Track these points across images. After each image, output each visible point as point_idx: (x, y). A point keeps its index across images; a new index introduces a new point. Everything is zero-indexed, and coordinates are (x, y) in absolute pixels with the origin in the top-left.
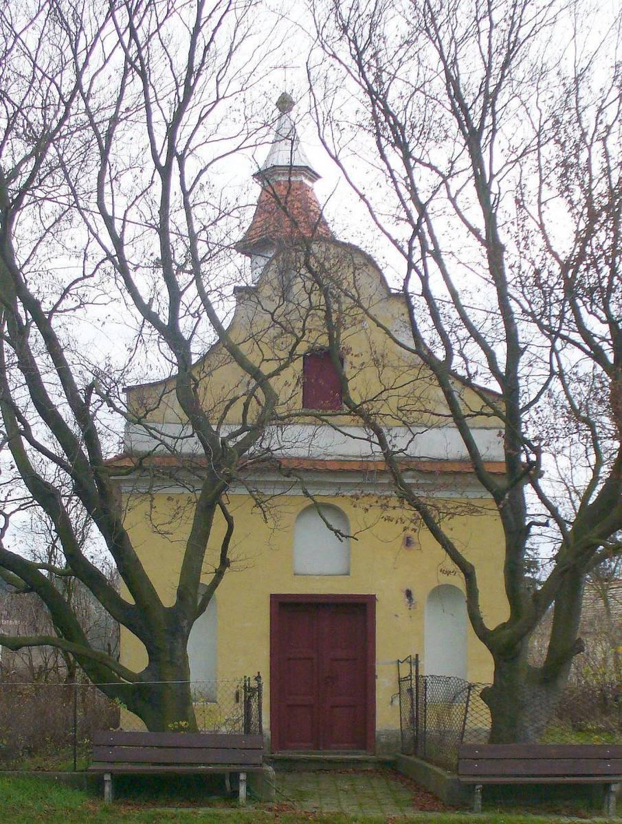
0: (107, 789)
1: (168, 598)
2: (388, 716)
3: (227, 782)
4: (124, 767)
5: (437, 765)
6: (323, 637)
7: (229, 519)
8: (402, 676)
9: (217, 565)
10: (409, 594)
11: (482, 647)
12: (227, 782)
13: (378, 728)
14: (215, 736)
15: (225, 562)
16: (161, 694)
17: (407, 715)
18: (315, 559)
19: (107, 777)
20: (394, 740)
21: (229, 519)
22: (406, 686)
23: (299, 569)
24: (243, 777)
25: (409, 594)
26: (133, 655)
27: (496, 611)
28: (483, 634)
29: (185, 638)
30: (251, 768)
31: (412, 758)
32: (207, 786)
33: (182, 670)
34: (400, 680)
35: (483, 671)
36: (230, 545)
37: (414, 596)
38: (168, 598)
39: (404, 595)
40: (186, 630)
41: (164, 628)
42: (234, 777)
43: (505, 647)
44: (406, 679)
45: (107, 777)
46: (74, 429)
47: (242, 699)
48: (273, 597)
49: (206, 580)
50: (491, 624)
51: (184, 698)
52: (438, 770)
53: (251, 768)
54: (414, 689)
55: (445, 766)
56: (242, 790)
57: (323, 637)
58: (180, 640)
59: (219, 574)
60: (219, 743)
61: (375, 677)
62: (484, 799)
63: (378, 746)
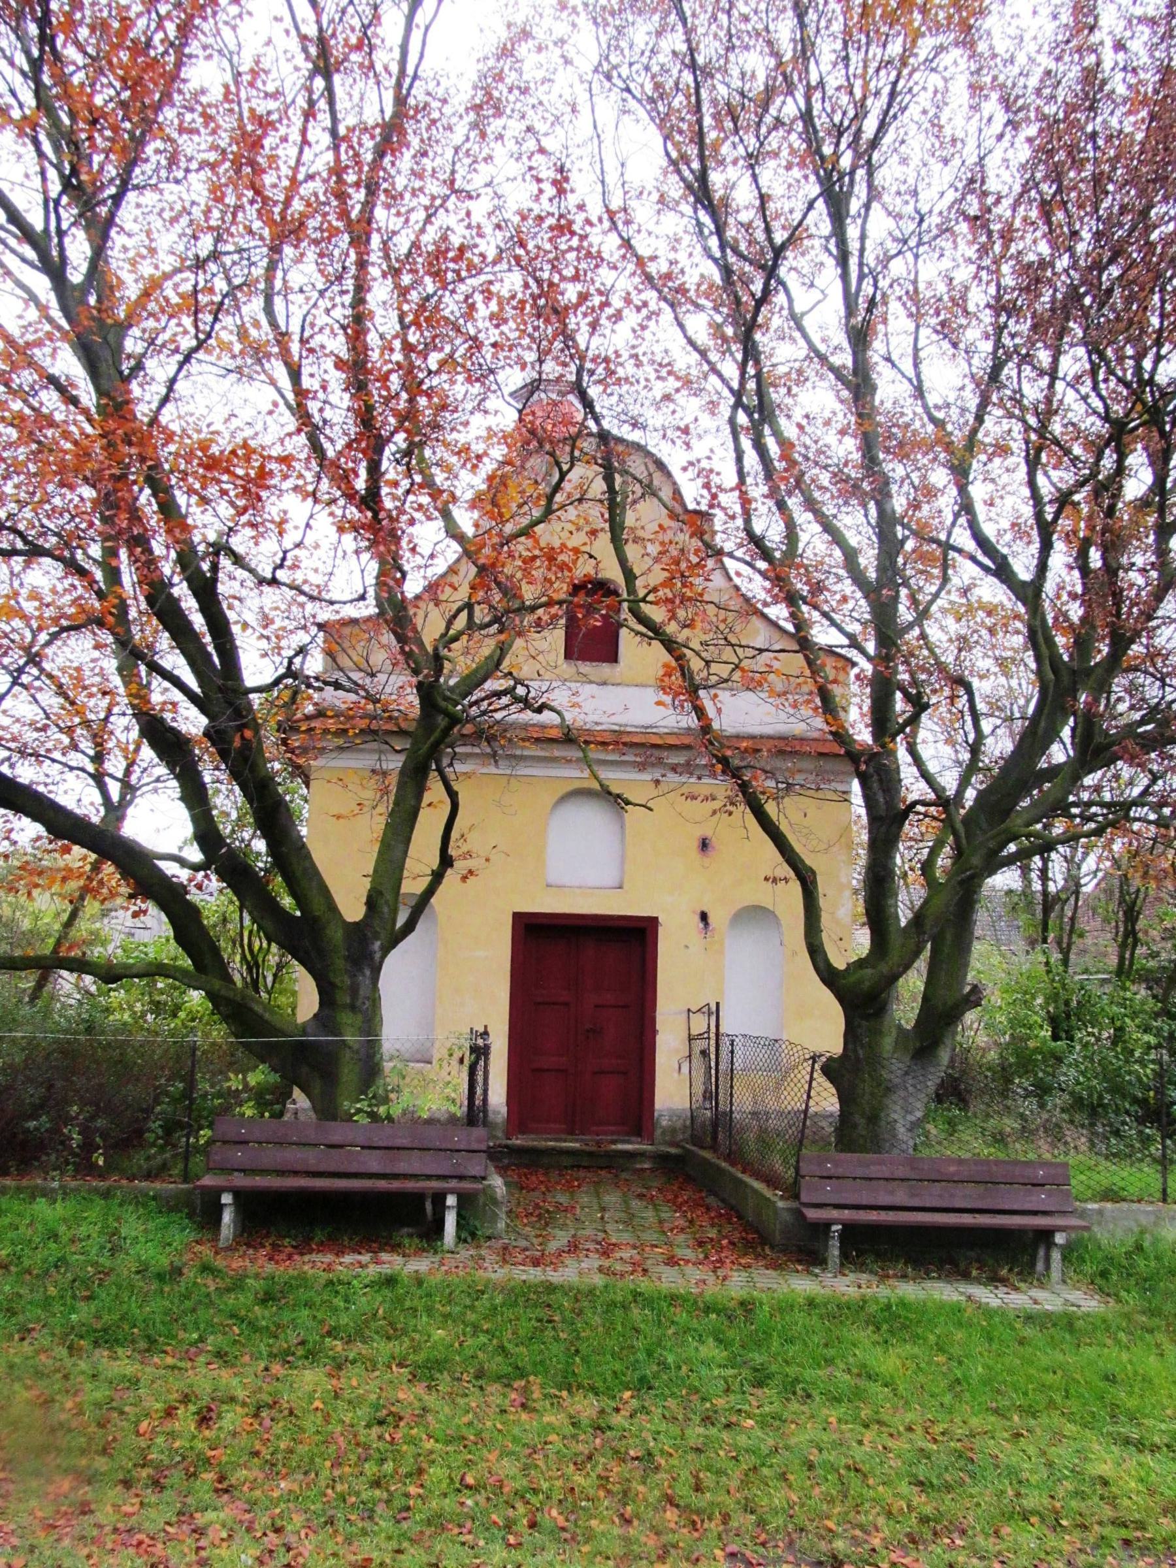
0: (227, 1217)
1: (352, 909)
2: (673, 1091)
3: (429, 1207)
4: (259, 1181)
5: (758, 1176)
6: (584, 972)
7: (453, 795)
8: (694, 1032)
9: (435, 863)
10: (704, 917)
11: (827, 997)
12: (429, 1207)
13: (658, 1105)
14: (414, 1121)
15: (446, 861)
16: (328, 1062)
17: (699, 1089)
18: (581, 864)
19: (226, 1199)
20: (679, 1124)
21: (453, 795)
22: (699, 1045)
23: (553, 878)
24: (451, 1200)
25: (704, 917)
26: (302, 997)
27: (850, 942)
28: (829, 976)
29: (377, 970)
30: (466, 1185)
31: (707, 1154)
32: (388, 1215)
33: (371, 1022)
34: (691, 1039)
35: (824, 1028)
36: (454, 835)
37: (711, 920)
38: (352, 909)
39: (697, 918)
40: (377, 956)
41: (347, 955)
42: (439, 1199)
43: (861, 996)
44: (700, 1036)
45: (226, 1199)
46: (198, 621)
47: (467, 1062)
48: (517, 917)
49: (412, 886)
50: (839, 962)
51: (371, 1068)
52: (758, 1185)
53: (466, 1185)
54: (711, 1050)
55: (772, 1181)
56: (450, 1220)
57: (584, 972)
58: (368, 973)
59: (438, 877)
60: (424, 1134)
61: (654, 1032)
62: (845, 1255)
63: (658, 1132)
